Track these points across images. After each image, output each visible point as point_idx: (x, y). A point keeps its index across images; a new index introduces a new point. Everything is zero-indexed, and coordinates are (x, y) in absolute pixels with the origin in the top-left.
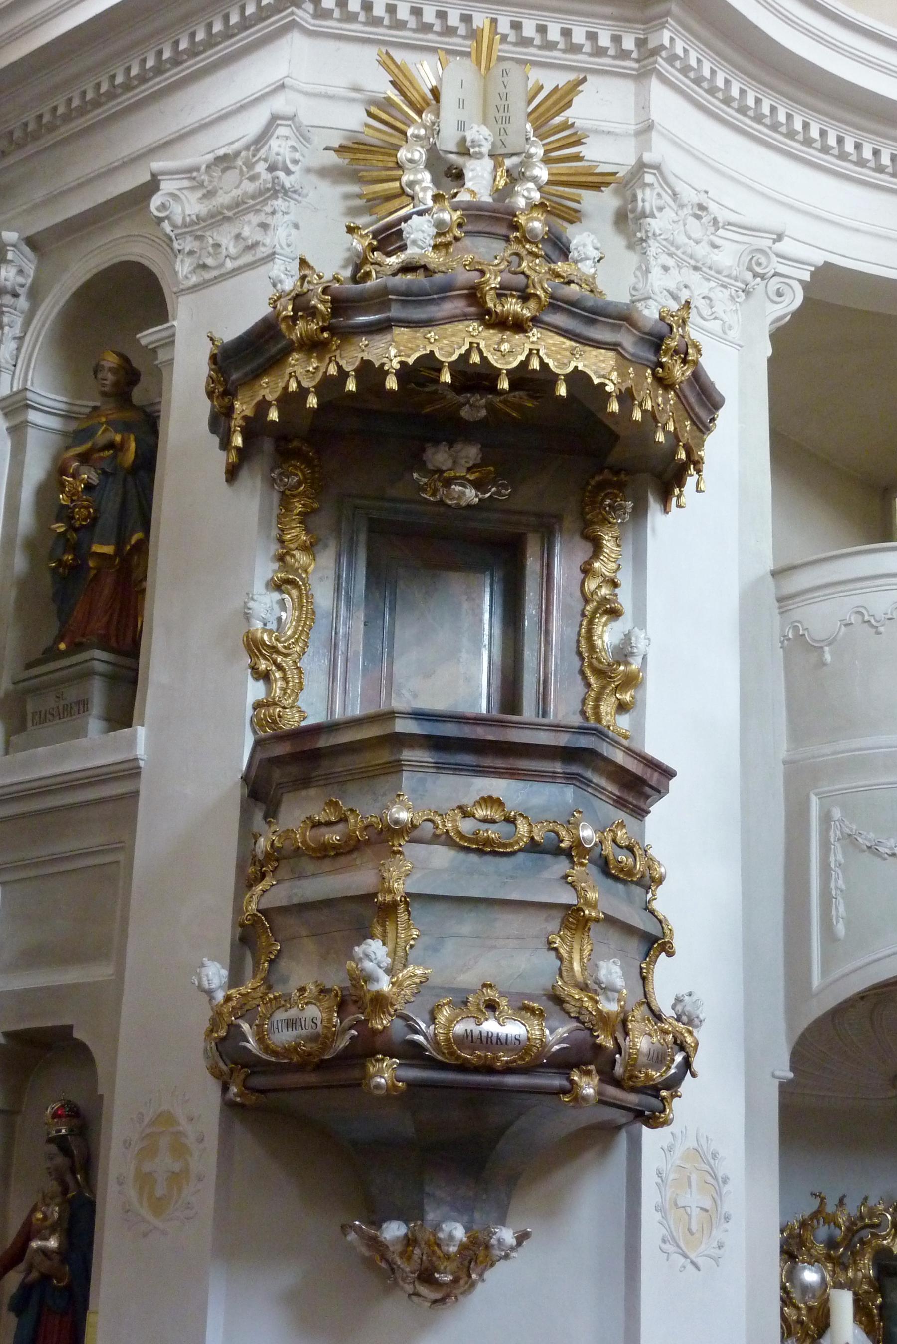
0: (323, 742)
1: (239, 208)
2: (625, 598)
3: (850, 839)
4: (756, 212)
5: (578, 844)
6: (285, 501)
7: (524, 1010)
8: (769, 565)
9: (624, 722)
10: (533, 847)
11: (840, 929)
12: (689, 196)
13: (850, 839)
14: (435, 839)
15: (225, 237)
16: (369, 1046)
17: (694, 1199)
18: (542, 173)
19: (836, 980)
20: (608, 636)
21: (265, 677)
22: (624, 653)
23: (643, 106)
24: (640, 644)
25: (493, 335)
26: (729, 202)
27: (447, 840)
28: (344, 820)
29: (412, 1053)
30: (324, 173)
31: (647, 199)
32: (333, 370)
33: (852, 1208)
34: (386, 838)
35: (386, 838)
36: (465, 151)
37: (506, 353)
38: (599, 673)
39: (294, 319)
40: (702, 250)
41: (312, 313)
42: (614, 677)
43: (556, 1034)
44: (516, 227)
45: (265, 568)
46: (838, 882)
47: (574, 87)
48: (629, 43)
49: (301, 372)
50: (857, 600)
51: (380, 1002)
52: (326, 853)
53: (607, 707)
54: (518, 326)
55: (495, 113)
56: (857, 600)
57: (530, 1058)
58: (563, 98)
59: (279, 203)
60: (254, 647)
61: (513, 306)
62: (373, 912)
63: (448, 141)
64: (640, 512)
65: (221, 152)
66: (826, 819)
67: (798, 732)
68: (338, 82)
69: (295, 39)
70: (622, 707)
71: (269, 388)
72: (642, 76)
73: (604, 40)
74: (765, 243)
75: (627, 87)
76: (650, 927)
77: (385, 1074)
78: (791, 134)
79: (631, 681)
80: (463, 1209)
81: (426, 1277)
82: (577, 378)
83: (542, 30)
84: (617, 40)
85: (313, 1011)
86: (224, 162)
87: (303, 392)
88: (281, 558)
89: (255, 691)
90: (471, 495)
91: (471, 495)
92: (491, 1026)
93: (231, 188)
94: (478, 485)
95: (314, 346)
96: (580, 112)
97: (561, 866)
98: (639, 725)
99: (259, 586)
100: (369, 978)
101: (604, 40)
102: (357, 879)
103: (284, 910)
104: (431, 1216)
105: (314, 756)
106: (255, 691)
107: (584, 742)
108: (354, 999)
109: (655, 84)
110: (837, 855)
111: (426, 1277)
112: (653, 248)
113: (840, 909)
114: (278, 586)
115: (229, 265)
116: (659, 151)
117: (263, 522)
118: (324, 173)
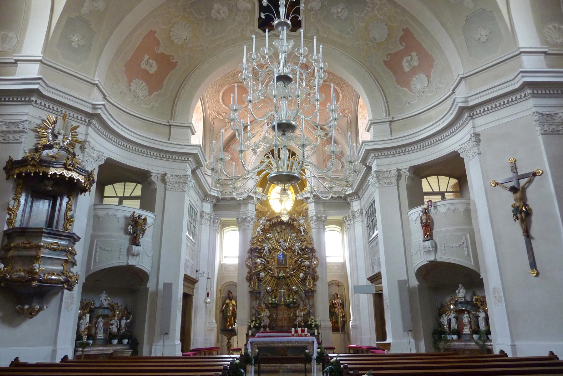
0: (28, 230)
1: (15, 132)
2: (73, 208)
3: (100, 247)
4: (102, 149)
5: (69, 250)
6: (18, 185)
7: (58, 275)
8: (93, 203)
9: (70, 227)
10: (62, 250)
11: (97, 261)
12: (92, 145)
13: (100, 247)
14: (46, 248)
15: (11, 136)
16: (33, 279)
17: (69, 301)
18: (70, 138)
19: (94, 268)
20: (70, 213)
21: (10, 215)
22: (72, 217)
23: (87, 130)
24: (75, 215)
25: (66, 171)
26: (97, 147)
27: (49, 248)
28: (30, 243)
29: (40, 281)
30: (32, 130)
31: (86, 146)
32: (37, 171)
33: (87, 301)
34: (38, 247)
35: (38, 247)
36: (59, 133)
37: (67, 174)
38: (68, 220)
39: (31, 161)
40: (92, 154)
41: (36, 161)
42: (69, 220)
43: (62, 278)
44: (68, 151)
45: (12, 196)
46: (98, 254)
47: (78, 127)
48: (87, 121)
49: (30, 169)
50: (107, 212)
51: (36, 273)
52: (25, 248)
53: (68, 225)
54: (70, 170)
55: (65, 128)
56: (107, 212)
57: (58, 282)
58: (76, 128)
59: (24, 134)
60: (9, 209)
61: (70, 167)
62: (36, 258)
63: (56, 131)
64: (77, 195)
65: (12, 121)
66: (97, 244)
67: (94, 229)
68: (37, 116)
69: (31, 106)
70: (70, 225)
71: (23, 170)
72: (88, 126)
73: (83, 119)
74: (101, 154)
75: (85, 126)
76: (74, 262)
77: (35, 284)
78: (107, 137)
79: (72, 221)
80: (39, 304)
81: (30, 314)
82: (78, 180)
83: (73, 115)
84: (85, 119)
85: (22, 274)
86: (13, 123)
87: (30, 173)
88: (16, 195)
89: (8, 217)
90: (51, 189)
91: (51, 189)
92: (53, 277)
93: (13, 128)
94: (52, 187)
95: (33, 166)
96: (78, 130)
97: (65, 253)
98: (72, 228)
99: (11, 199)
100: (35, 269)
101: (83, 119)
102: (33, 253)
103: (16, 256)
104: (34, 305)
105: (25, 232)
106: (8, 217)
107: (71, 235)
108: (32, 272)
109: (90, 128)
110: (98, 250)
111: (30, 314)
112: (86, 153)
113: (97, 258)
114: (14, 199)
115: (11, 141)
116: (89, 139)
117: (13, 188)
118: (32, 130)
